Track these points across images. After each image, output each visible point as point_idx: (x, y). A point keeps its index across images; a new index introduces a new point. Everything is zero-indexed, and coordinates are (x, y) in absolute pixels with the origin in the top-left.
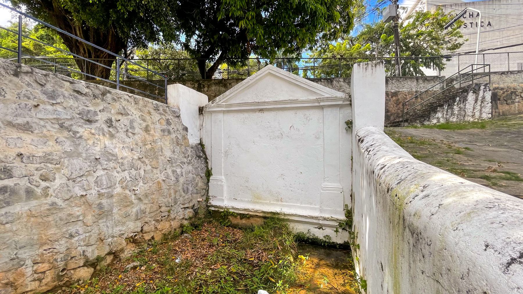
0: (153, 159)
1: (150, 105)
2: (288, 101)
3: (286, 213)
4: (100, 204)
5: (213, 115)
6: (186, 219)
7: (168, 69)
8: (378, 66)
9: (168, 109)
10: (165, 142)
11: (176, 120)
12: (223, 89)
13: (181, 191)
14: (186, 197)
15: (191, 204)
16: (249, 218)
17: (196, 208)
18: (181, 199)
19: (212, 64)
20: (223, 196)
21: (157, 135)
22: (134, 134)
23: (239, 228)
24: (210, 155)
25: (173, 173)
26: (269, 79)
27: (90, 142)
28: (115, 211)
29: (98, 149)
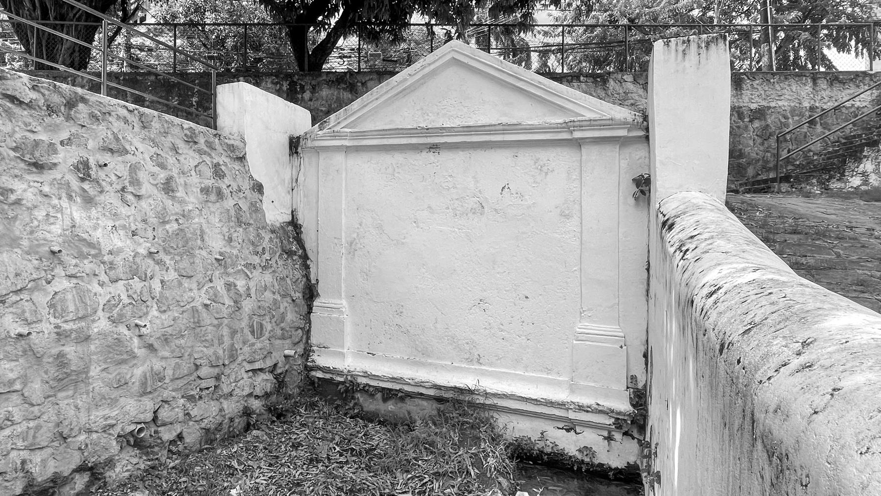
0: (181, 255)
1: (176, 130)
2: (497, 128)
3: (488, 391)
4: (61, 355)
5: (323, 156)
6: (257, 397)
7: (223, 46)
8: (713, 46)
9: (217, 140)
10: (211, 218)
11: (237, 166)
12: (347, 95)
13: (247, 331)
14: (258, 345)
15: (269, 363)
16: (402, 399)
17: (279, 371)
18: (246, 349)
19: (323, 35)
20: (343, 347)
21: (193, 200)
22: (138, 197)
23: (380, 423)
24: (315, 250)
25: (228, 290)
26: (453, 75)
27: (40, 214)
28: (94, 371)
29: (57, 229)
